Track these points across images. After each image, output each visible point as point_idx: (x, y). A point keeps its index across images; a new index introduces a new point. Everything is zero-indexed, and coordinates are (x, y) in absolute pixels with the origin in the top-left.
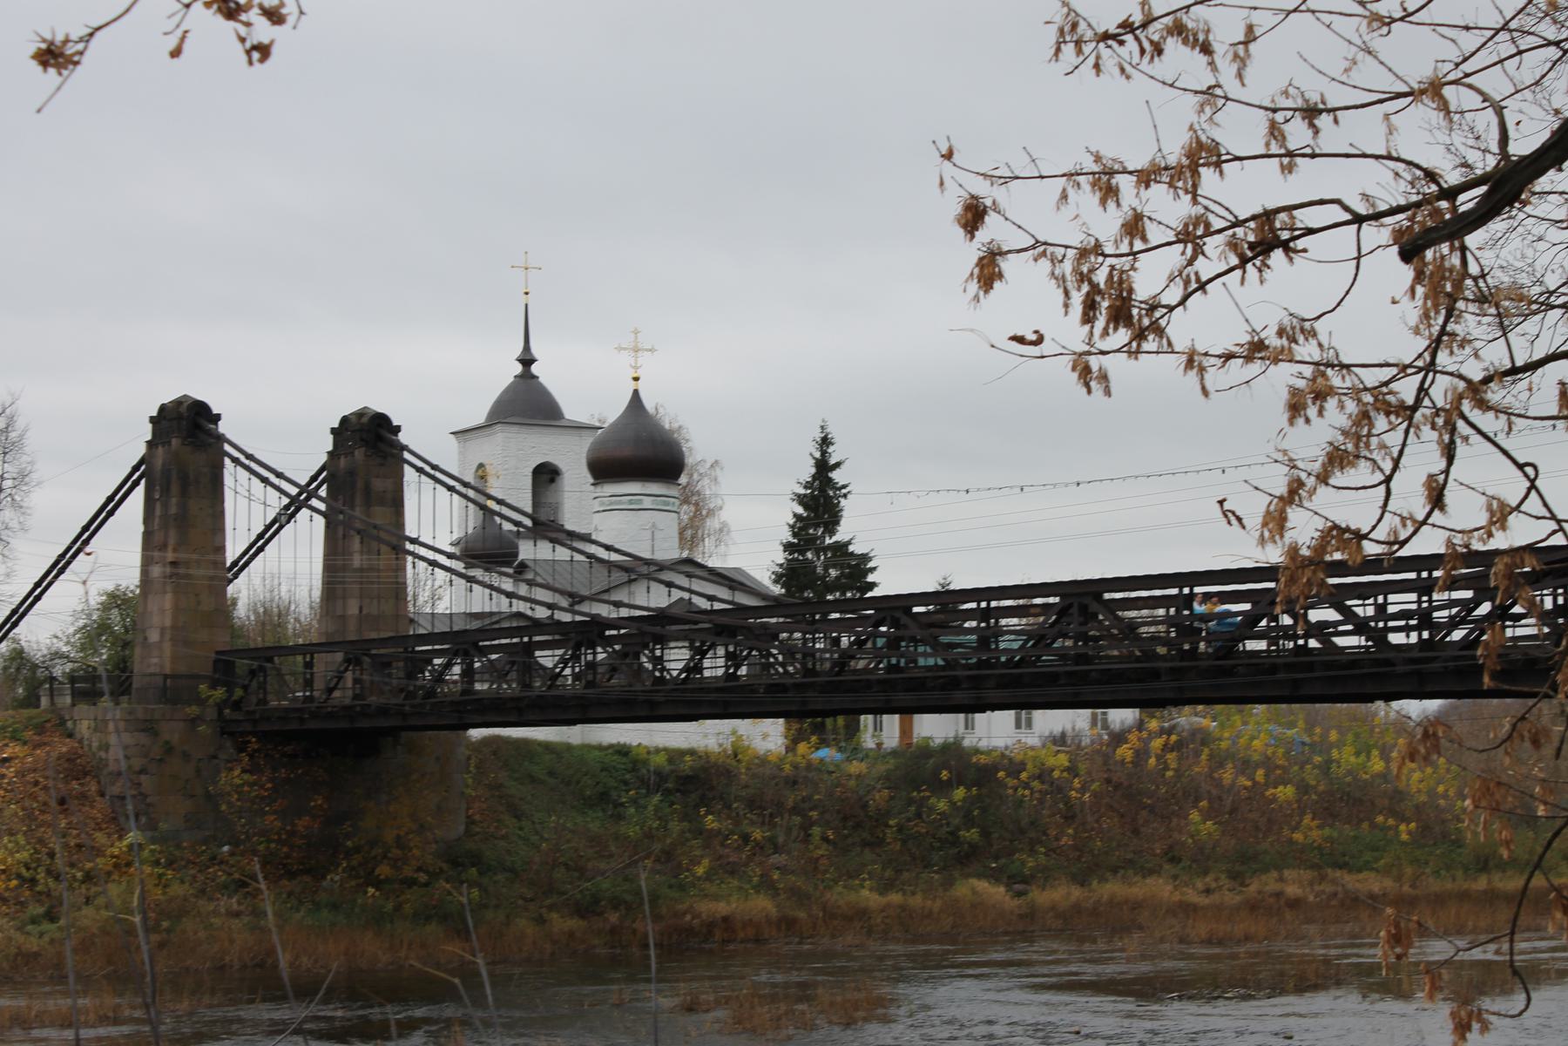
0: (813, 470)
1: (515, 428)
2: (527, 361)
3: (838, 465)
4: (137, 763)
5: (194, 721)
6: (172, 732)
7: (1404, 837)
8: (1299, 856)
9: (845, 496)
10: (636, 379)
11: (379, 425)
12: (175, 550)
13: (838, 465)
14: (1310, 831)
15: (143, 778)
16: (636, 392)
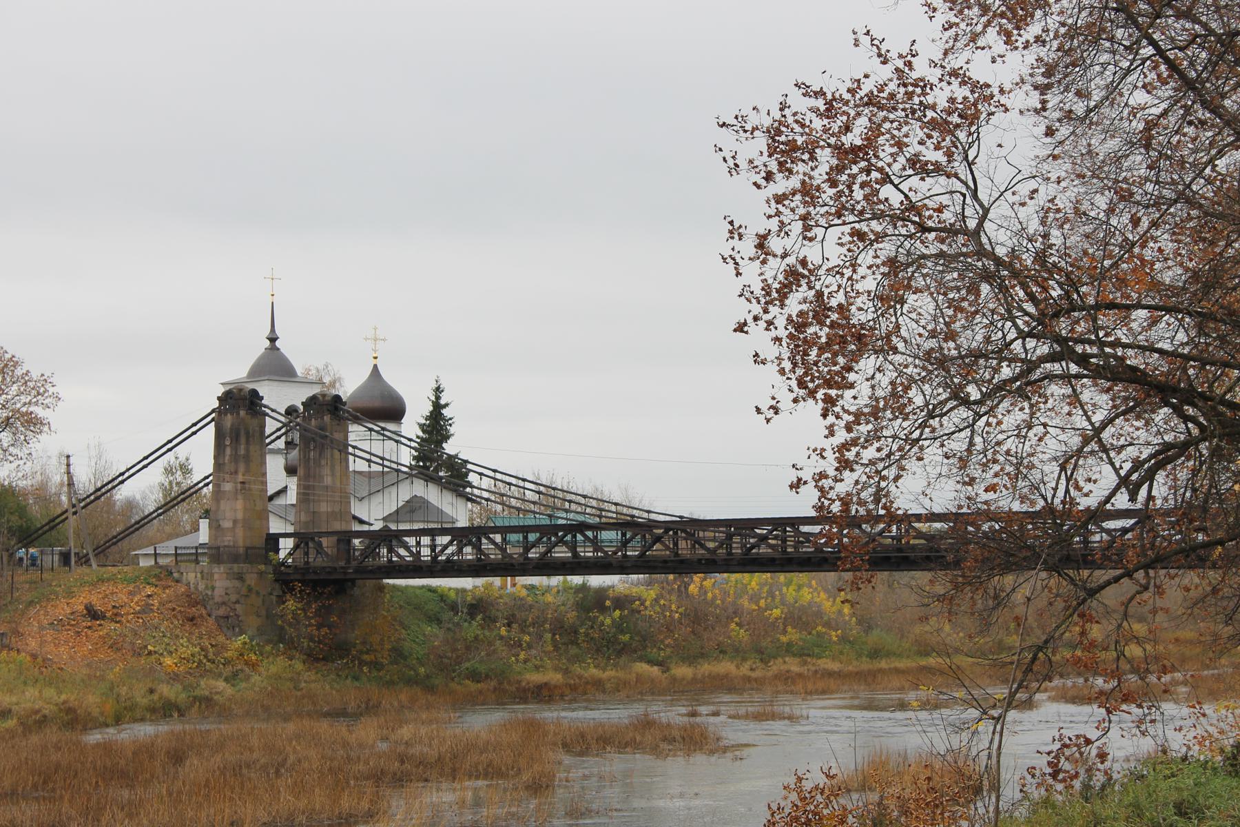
0: (431, 408)
1: (276, 383)
2: (273, 340)
3: (447, 405)
4: (233, 598)
5: (261, 574)
6: (251, 579)
7: (835, 639)
8: (789, 649)
9: (450, 425)
10: (376, 358)
11: (336, 402)
12: (243, 475)
13: (447, 405)
14: (792, 635)
15: (237, 606)
16: (375, 366)
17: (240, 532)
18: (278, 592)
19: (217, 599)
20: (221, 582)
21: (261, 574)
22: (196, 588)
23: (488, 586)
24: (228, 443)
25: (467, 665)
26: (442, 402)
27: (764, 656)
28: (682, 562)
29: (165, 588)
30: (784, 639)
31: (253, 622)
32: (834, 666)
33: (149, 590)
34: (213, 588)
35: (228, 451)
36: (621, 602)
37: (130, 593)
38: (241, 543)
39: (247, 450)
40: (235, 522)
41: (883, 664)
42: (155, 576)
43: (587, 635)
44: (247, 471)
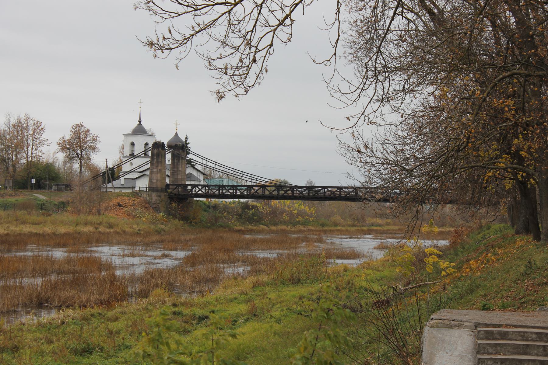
2: (140, 122)
4: (158, 202)
6: (163, 197)
14: (300, 219)
16: (176, 132)
17: (159, 183)
18: (169, 201)
19: (153, 202)
20: (154, 197)
21: (165, 195)
22: (146, 199)
23: (247, 202)
24: (155, 157)
25: (219, 223)
26: (187, 142)
27: (294, 224)
28: (295, 197)
29: (138, 198)
30: (297, 220)
31: (163, 209)
32: (313, 228)
33: (133, 199)
34: (152, 199)
35: (155, 160)
36: (254, 207)
37: (128, 200)
38: (159, 187)
39: (161, 160)
40: (157, 180)
41: (326, 228)
42: (134, 195)
43: (245, 216)
44: (161, 166)
